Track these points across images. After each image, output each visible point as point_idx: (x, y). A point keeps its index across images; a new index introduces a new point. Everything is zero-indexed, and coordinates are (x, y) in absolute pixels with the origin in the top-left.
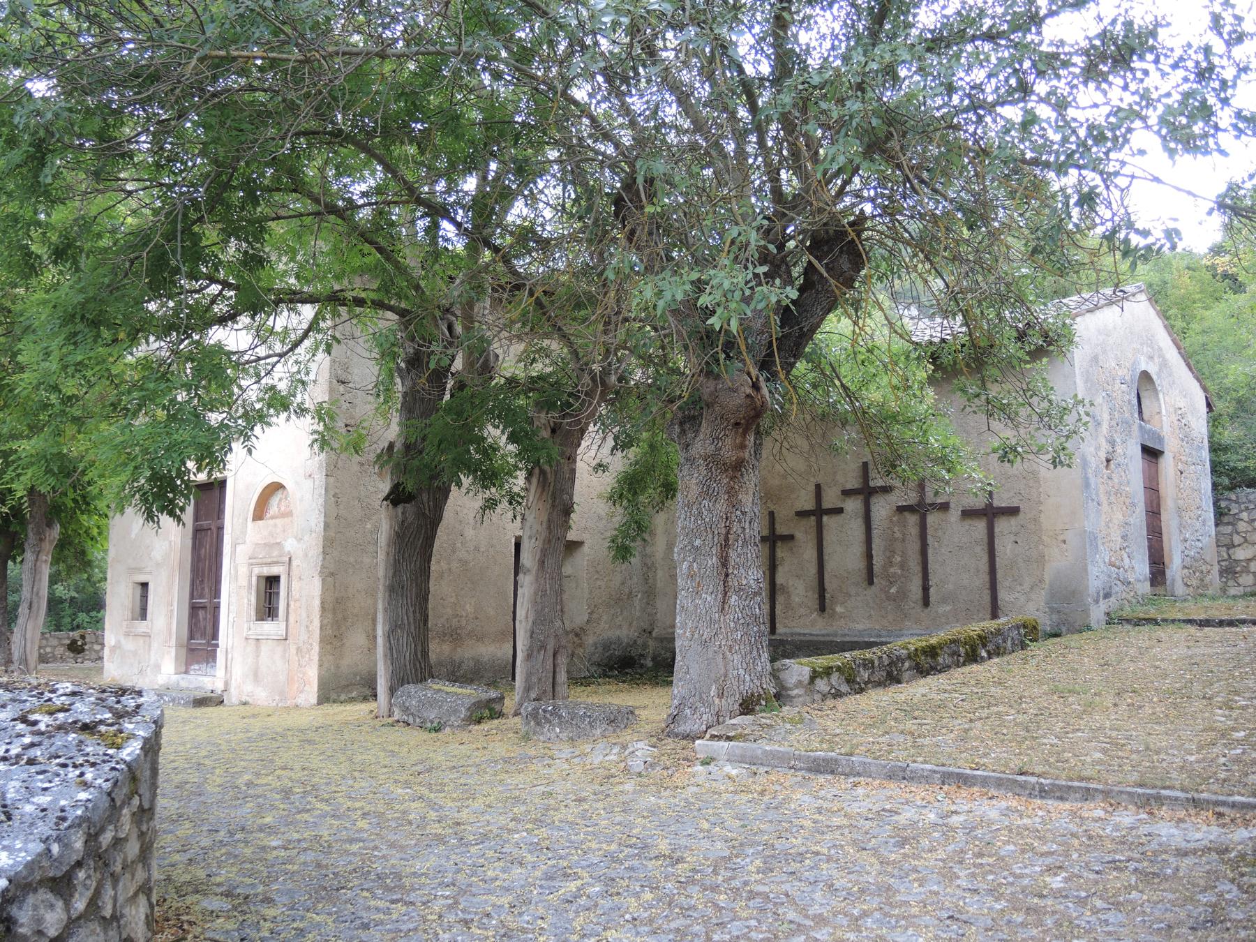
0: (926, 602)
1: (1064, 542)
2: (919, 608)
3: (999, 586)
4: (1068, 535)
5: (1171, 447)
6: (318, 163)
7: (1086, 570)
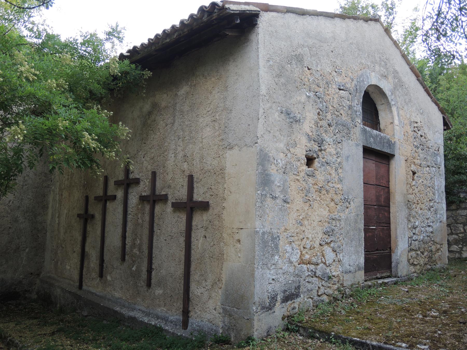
0: (149, 285)
1: (239, 241)
2: (145, 288)
3: (192, 278)
4: (243, 235)
5: (403, 153)
6: (23, 29)
7: (253, 275)
